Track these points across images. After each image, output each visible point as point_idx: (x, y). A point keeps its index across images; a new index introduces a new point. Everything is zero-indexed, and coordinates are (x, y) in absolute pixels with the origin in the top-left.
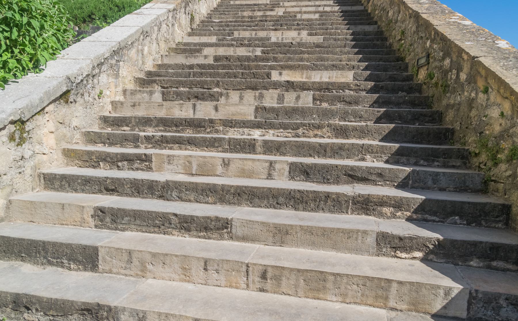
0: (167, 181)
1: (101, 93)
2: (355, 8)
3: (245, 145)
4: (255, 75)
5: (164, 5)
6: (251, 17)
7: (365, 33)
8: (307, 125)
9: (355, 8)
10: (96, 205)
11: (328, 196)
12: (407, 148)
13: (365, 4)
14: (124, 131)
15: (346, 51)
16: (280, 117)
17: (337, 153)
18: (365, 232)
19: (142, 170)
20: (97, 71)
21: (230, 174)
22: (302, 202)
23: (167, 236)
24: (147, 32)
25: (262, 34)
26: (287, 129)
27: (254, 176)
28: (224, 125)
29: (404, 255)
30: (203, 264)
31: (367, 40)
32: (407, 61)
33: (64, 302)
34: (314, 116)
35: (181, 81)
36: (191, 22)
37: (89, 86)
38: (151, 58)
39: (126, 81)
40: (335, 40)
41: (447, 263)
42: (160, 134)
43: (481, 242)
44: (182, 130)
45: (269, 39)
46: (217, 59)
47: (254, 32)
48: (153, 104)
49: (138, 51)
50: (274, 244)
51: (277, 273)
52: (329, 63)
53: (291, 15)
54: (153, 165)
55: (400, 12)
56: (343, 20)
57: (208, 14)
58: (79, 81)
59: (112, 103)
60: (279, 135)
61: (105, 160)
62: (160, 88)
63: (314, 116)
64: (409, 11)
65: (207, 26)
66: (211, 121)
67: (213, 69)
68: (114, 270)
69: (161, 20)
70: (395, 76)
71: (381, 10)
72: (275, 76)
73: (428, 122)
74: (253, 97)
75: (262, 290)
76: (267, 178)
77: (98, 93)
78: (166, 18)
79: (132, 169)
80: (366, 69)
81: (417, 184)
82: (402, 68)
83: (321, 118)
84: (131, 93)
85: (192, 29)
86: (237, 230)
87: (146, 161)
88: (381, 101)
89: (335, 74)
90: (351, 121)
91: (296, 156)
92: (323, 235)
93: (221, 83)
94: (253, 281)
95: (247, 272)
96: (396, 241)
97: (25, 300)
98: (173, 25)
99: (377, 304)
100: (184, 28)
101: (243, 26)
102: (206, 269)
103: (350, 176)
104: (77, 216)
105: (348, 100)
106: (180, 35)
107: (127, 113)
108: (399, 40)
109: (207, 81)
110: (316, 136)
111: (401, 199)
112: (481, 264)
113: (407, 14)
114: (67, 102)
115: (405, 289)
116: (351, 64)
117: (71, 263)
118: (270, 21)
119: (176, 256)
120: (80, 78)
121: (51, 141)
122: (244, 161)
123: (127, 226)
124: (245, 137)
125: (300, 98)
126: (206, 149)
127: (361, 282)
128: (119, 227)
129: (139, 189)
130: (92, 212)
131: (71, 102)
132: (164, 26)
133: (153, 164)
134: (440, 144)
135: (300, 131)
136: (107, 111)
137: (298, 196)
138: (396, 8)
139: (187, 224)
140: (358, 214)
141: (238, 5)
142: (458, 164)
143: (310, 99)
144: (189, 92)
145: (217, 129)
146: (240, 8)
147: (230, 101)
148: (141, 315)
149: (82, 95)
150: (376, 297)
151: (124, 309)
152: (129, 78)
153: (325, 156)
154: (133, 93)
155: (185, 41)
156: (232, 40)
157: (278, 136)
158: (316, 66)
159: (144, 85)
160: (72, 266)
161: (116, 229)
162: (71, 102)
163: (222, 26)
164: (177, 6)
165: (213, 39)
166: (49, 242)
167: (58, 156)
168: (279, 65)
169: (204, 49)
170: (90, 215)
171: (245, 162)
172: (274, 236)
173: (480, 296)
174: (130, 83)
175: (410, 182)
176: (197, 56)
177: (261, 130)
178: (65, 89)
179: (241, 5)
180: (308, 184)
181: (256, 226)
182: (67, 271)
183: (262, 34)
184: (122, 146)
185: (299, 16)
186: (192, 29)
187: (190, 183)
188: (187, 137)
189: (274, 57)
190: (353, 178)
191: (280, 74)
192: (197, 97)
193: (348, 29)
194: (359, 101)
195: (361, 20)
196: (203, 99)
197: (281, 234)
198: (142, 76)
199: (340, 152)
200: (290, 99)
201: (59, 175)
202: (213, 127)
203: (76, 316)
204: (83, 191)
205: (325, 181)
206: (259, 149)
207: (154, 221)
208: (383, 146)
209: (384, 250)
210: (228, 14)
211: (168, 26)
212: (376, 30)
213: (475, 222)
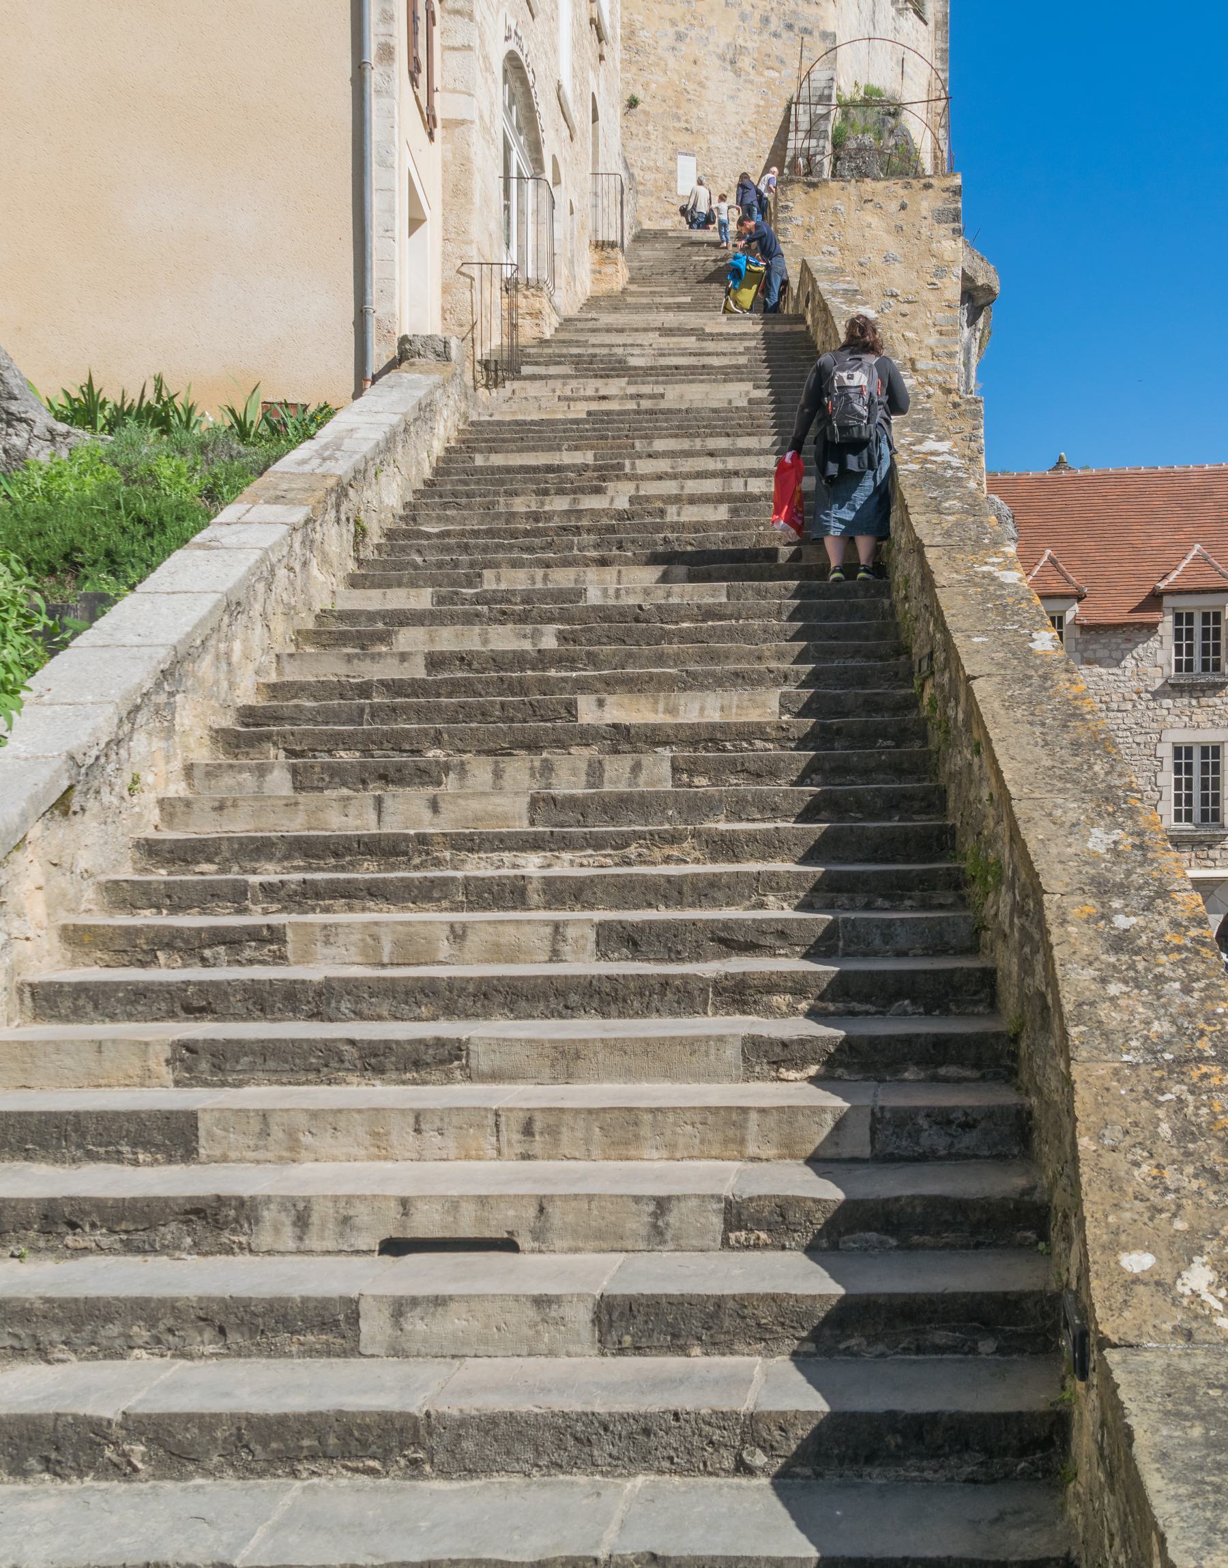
0: (328, 980)
1: (135, 782)
4: (535, 711)
5: (278, 509)
6: (535, 516)
10: (176, 1037)
11: (665, 983)
12: (849, 873)
14: (202, 873)
16: (590, 820)
18: (721, 1039)
19: (263, 963)
20: (127, 727)
21: (468, 956)
22: (615, 1000)
23: (335, 1088)
24: (238, 604)
25: (563, 578)
26: (602, 847)
28: (453, 847)
29: (792, 1075)
30: (412, 1121)
33: (149, 1201)
35: (340, 733)
37: (110, 768)
38: (251, 667)
39: (192, 741)
41: (866, 1079)
42: (298, 876)
43: (918, 1035)
44: (351, 863)
45: (580, 593)
46: (435, 662)
47: (539, 573)
48: (271, 802)
49: (217, 657)
50: (555, 1080)
51: (552, 1120)
53: (649, 507)
54: (290, 950)
57: (406, 505)
58: (92, 761)
59: (161, 802)
61: (169, 946)
62: (282, 754)
65: (403, 549)
66: (423, 839)
67: (426, 693)
68: (233, 1155)
69: (274, 560)
72: (588, 712)
73: (918, 812)
75: (526, 1157)
76: (551, 961)
77: (129, 781)
78: (285, 551)
79: (239, 963)
81: (853, 948)
84: (208, 774)
86: (481, 1061)
87: (271, 942)
88: (827, 766)
90: (754, 820)
91: (617, 908)
92: (646, 1053)
93: (446, 736)
94: (509, 1142)
95: (497, 1125)
96: (778, 1050)
97: (67, 1210)
98: (305, 564)
99: (727, 1154)
100: (335, 564)
101: (511, 548)
102: (418, 1131)
103: (721, 941)
104: (134, 1066)
105: (752, 767)
106: (327, 588)
107: (203, 827)
110: (667, 860)
111: (805, 975)
112: (922, 1075)
114: (65, 814)
115: (771, 1121)
117: (139, 1150)
118: (589, 531)
119: (359, 1111)
120: (94, 752)
121: (37, 908)
123: (247, 1076)
124: (504, 872)
127: (697, 1119)
128: (230, 1079)
129: (261, 1000)
130: (168, 1053)
131: (75, 813)
132: (282, 573)
133: (290, 946)
134: (931, 862)
135: (632, 851)
136: (151, 825)
137: (607, 987)
139: (375, 1060)
140: (728, 1014)
142: (950, 901)
143: (666, 769)
144: (363, 766)
146: (502, 482)
147: (470, 781)
148: (301, 1206)
149: (98, 792)
150: (726, 1142)
151: (269, 1199)
152: (198, 733)
153: (680, 903)
154: (212, 772)
156: (479, 599)
157: (582, 865)
158: (693, 675)
159: (238, 747)
160: (141, 1157)
161: (223, 1084)
162: (75, 813)
163: (447, 549)
164: (314, 509)
165: (422, 599)
166: (88, 1114)
167: (50, 942)
168: (601, 679)
169: (397, 633)
170: (162, 1059)
171: (501, 928)
172: (553, 1066)
173: (888, 1115)
174: (201, 745)
175: (841, 944)
176: (380, 654)
178: (65, 784)
179: (508, 470)
180: (638, 964)
181: (517, 1048)
182: (130, 1168)
183: (563, 578)
184: (204, 912)
185: (672, 514)
187: (379, 979)
188: (365, 881)
189: (589, 654)
190: (728, 946)
191: (601, 704)
192: (384, 778)
194: (778, 769)
196: (401, 781)
197: (567, 1060)
198: (228, 721)
199: (711, 892)
200: (618, 776)
201: (69, 984)
203: (173, 1226)
204: (130, 1017)
206: (534, 898)
207: (305, 1058)
208: (799, 874)
209: (757, 1069)
210: (468, 507)
211: (291, 569)
213: (939, 1007)
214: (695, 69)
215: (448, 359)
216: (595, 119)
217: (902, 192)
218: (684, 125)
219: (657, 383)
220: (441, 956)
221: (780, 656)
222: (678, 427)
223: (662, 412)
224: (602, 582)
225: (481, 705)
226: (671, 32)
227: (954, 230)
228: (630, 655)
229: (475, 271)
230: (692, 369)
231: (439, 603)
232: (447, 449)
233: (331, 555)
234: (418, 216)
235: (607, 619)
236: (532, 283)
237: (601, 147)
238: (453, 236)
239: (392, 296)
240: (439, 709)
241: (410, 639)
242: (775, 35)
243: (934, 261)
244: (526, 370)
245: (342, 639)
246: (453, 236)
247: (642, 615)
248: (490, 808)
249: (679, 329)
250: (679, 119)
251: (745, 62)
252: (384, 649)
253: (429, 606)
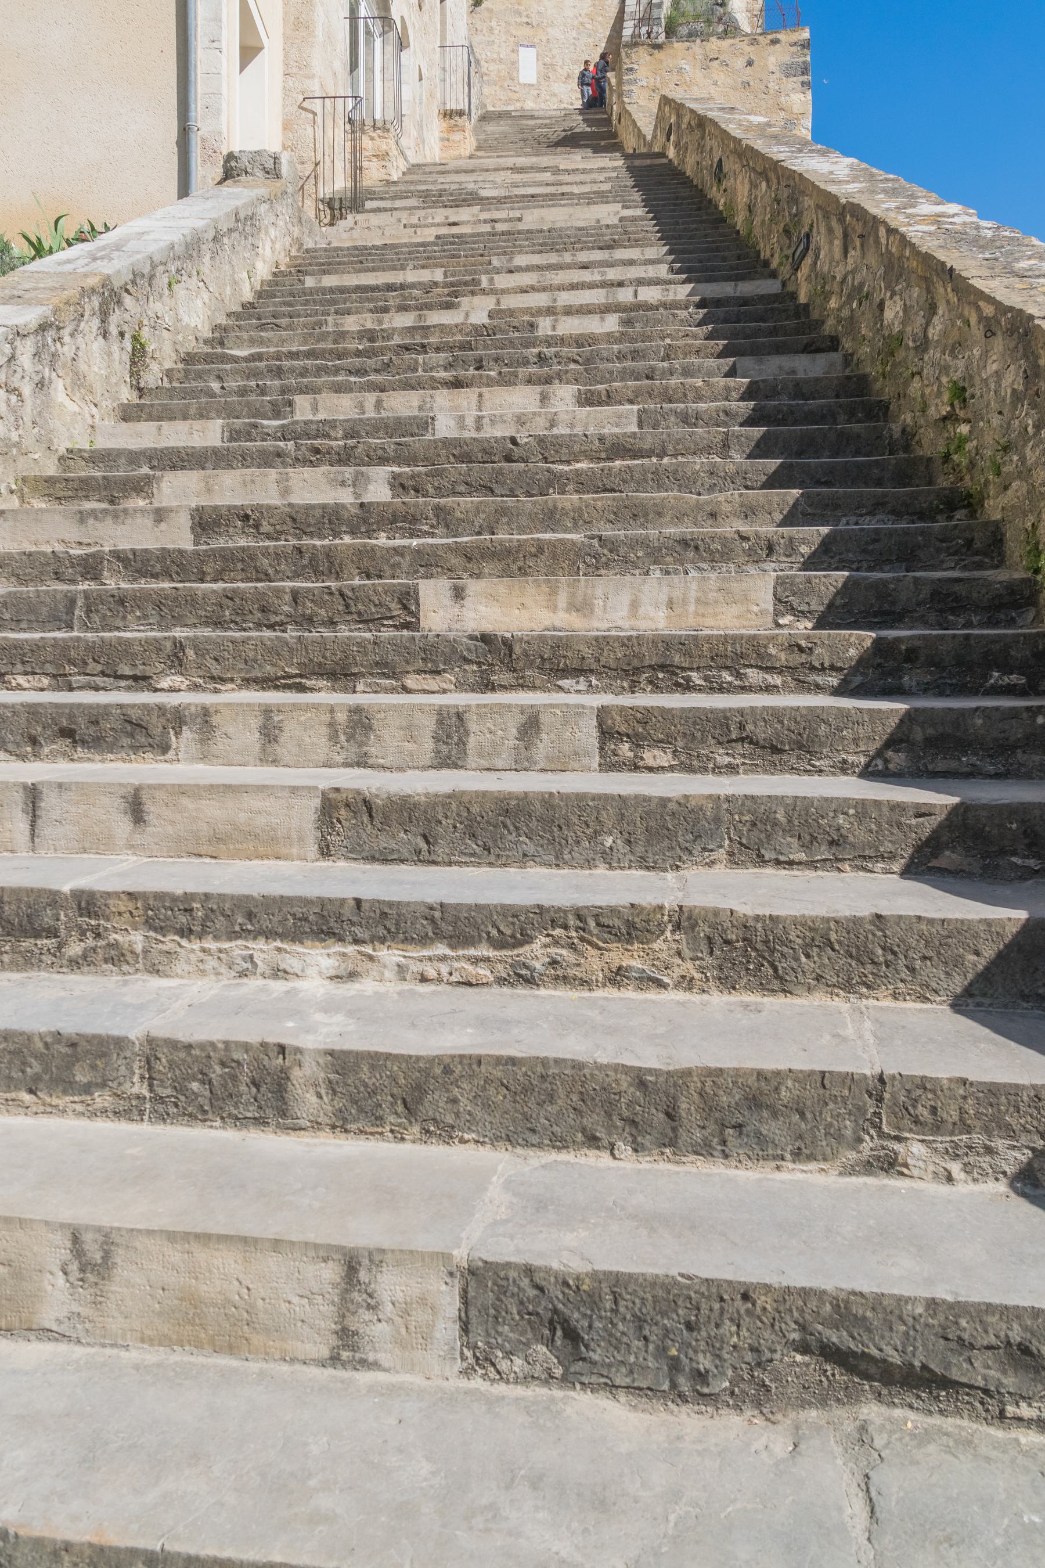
2: (747, 288)
3: (234, 1078)
6: (371, 336)
7: (797, 384)
8: (572, 922)
9: (747, 288)
13: (785, 271)
15: (731, 468)
17: (739, 1127)
21: (116, 1324)
25: (403, 404)
26: (468, 941)
27: (257, 1340)
31: (811, 417)
32: (997, 516)
34: (609, 841)
35: (17, 645)
36: (133, 363)
40: (685, 419)
45: (426, 424)
46: (206, 522)
47: (371, 398)
52: (668, 531)
53: (515, 322)
55: (932, 309)
56: (709, 337)
57: (216, 328)
60: (431, 973)
63: (609, 841)
64: (978, 309)
65: (199, 376)
70: (956, 588)
71: (850, 298)
72: (439, 612)
74: (325, 731)
76: (334, 1360)
80: (823, 557)
82: (978, 545)
83: (639, 849)
85: (140, 390)
88: (918, 735)
89: (694, 586)
93: (190, 653)
98: (41, 385)
100: (99, 388)
101: (337, 371)
105: (762, 733)
108: (945, 419)
109: (128, 642)
113: (973, 320)
116: (757, 535)
118: (438, 350)
122: (195, 1247)
125: (538, 732)
126: (27, 1098)
138: (916, 292)
141: (331, 290)
145: (115, 945)
146: (334, 302)
153: (672, 1143)
155: (102, 443)
158: (613, 545)
163: (256, 374)
165: (209, 434)
169: (159, 480)
171: (201, 1254)
177: (338, 948)
179: (342, 290)
183: (403, 404)
185: (545, 326)
186: (140, 390)
189: (438, 509)
190: (851, 1370)
191: (458, 594)
193: (732, 373)
194: (814, 738)
195: (774, 332)
199: (753, 1123)
202: (98, 936)
205: (685, 1385)
206: (308, 1101)
212: (838, 372)
215: (278, 177)
217: (748, 49)
218: (526, 20)
219: (513, 209)
220: (48, 1316)
221: (749, 512)
222: (541, 245)
223: (519, 232)
224: (456, 408)
225: (261, 595)
227: (803, 84)
228: (502, 511)
229: (317, 106)
230: (551, 196)
231: (231, 439)
232: (275, 274)
233: (91, 378)
234: (251, 43)
235: (465, 458)
236: (379, 124)
237: (449, 26)
238: (294, 70)
239: (219, 112)
240: (192, 600)
241: (181, 491)
243: (783, 114)
244: (369, 205)
245: (84, 488)
246: (294, 70)
247: (517, 452)
248: (242, 817)
249: (532, 168)
250: (520, 15)
252: (141, 503)
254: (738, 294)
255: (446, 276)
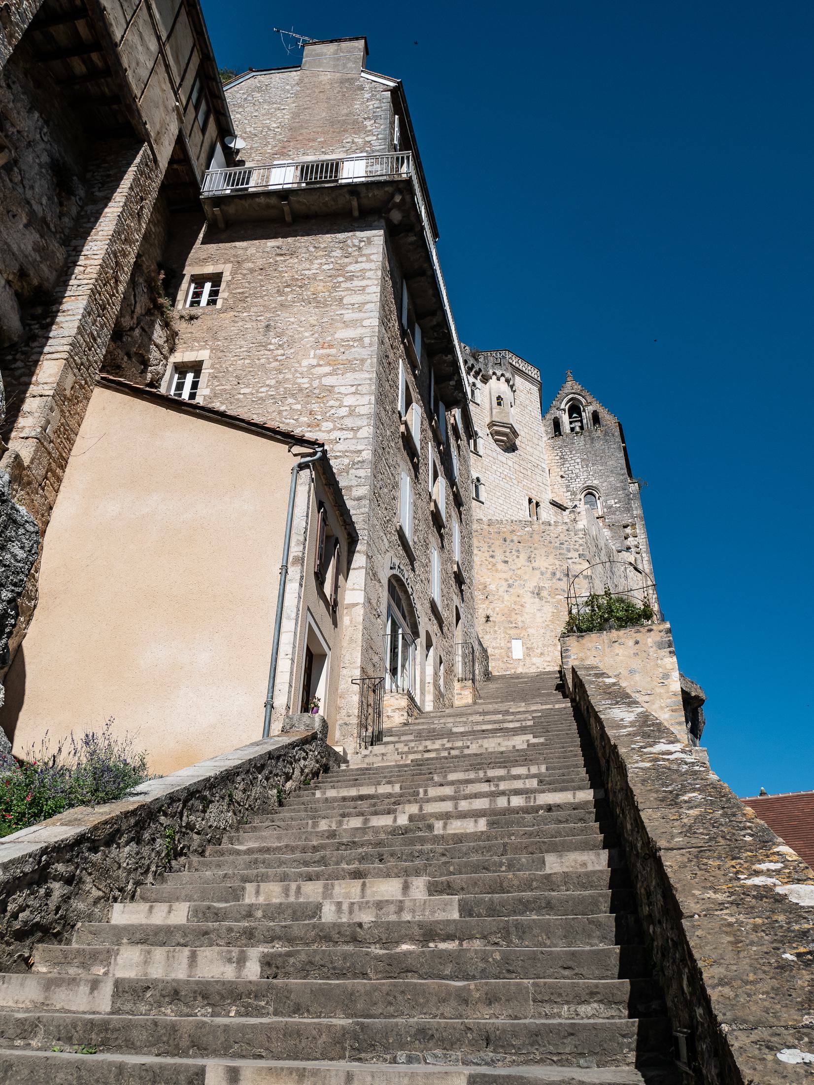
214: (518, 599)
216: (458, 618)
226: (505, 584)
227: (670, 652)
242: (559, 580)
243: (661, 670)
251: (544, 593)
253: (184, 921)
254: (577, 801)
255: (401, 789)
